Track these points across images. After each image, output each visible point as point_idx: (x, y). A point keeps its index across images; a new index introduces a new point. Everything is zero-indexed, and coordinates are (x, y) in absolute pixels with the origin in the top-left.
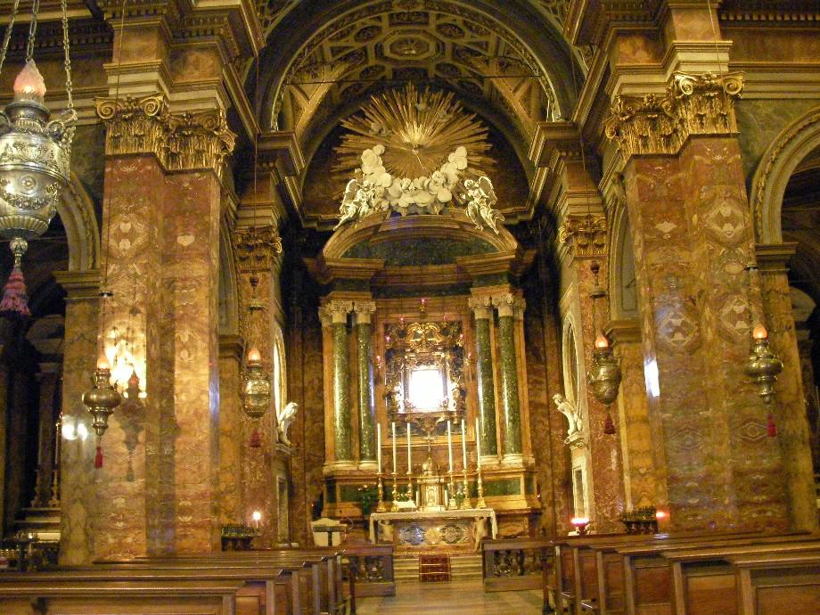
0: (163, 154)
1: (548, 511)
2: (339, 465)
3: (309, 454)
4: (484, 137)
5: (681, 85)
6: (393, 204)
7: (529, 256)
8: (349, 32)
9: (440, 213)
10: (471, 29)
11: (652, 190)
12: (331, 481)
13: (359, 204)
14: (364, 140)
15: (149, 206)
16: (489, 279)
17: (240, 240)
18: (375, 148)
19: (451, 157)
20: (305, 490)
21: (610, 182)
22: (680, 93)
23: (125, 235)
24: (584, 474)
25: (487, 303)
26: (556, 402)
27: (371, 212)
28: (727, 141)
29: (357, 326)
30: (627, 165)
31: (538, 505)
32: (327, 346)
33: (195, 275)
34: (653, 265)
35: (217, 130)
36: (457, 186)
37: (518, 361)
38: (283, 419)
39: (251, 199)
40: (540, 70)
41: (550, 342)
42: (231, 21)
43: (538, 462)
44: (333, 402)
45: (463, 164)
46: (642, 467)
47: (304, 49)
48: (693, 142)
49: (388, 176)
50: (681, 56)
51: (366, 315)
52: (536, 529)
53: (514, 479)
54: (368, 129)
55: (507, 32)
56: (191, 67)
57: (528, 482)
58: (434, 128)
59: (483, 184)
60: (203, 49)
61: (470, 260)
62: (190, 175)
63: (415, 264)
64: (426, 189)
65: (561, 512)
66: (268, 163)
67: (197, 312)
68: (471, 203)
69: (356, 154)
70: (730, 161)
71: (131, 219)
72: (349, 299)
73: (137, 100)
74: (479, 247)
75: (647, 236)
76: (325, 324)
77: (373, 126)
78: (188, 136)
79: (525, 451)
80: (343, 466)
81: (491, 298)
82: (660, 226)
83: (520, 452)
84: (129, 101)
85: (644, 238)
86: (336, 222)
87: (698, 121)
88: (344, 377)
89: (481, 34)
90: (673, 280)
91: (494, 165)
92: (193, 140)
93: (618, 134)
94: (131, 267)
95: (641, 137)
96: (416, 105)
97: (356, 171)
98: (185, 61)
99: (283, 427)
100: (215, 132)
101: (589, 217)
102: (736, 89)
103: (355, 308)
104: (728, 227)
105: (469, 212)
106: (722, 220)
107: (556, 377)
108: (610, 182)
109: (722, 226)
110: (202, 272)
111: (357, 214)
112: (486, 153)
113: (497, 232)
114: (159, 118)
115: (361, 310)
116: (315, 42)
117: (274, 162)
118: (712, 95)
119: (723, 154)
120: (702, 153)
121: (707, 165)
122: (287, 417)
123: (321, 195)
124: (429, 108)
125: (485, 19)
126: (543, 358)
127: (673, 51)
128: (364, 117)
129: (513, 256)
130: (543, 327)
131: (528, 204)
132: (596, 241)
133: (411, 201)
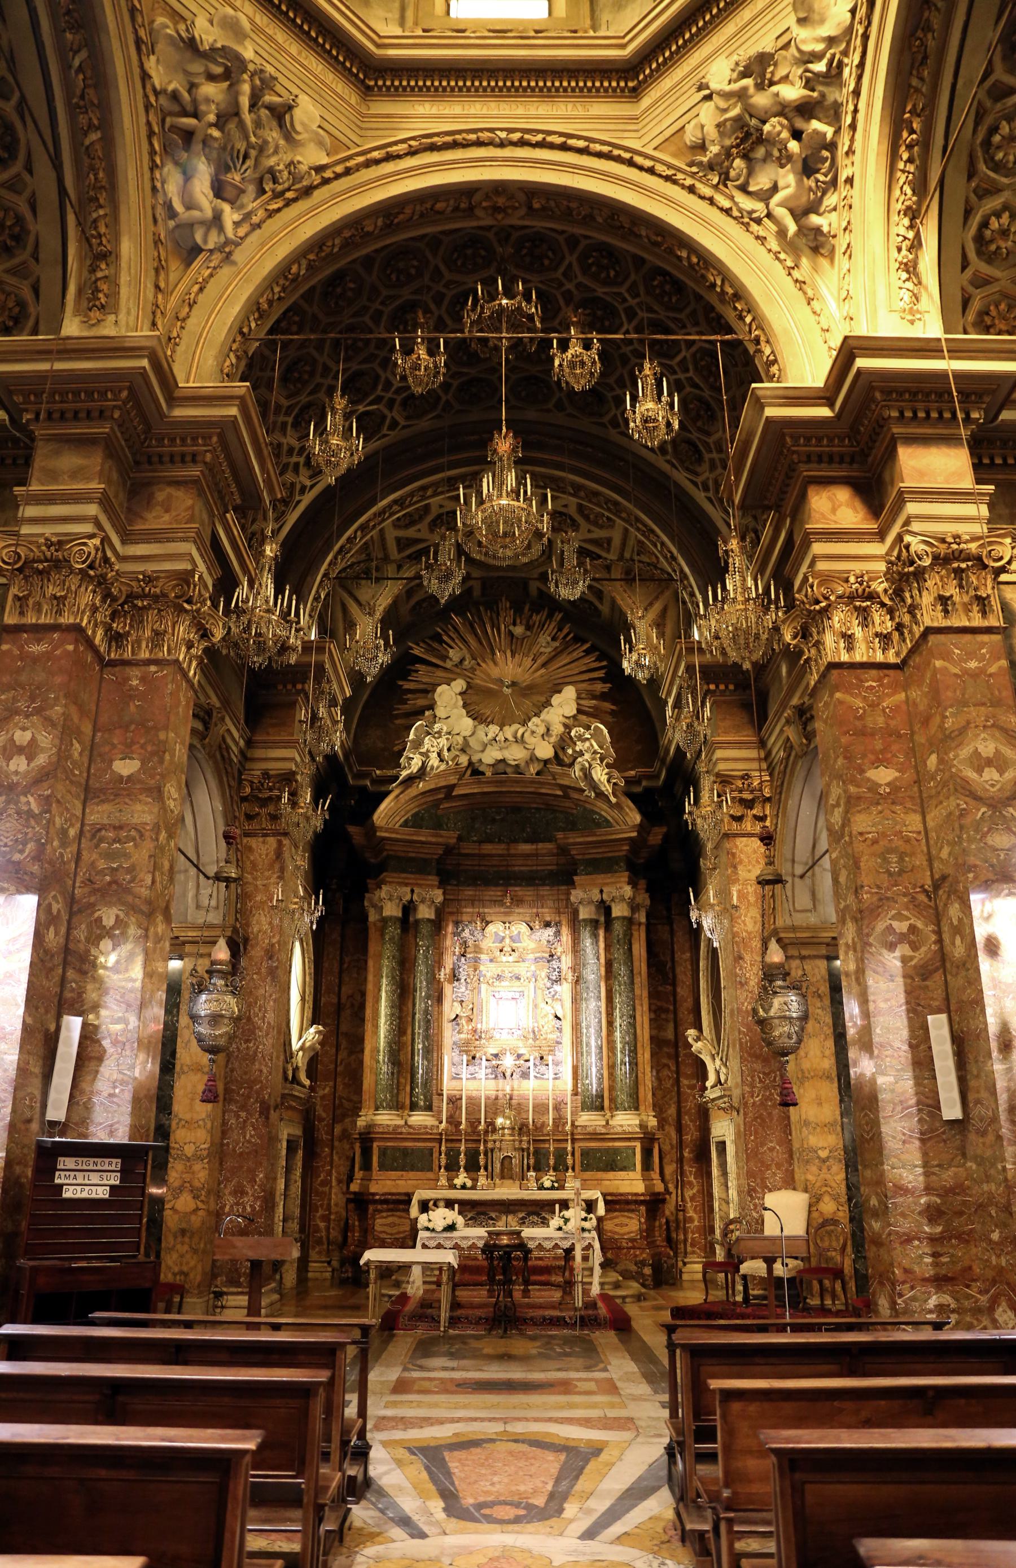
0: (100, 633)
1: (672, 1201)
2: (378, 1117)
3: (340, 1098)
4: (601, 674)
5: (912, 549)
6: (475, 759)
7: (657, 836)
8: (421, 518)
9: (538, 774)
10: (587, 518)
11: (861, 718)
12: (367, 1138)
13: (426, 755)
14: (440, 673)
15: (66, 706)
16: (600, 866)
17: (248, 790)
18: (453, 684)
19: (556, 699)
20: (332, 1148)
21: (783, 720)
22: (912, 563)
23: (20, 750)
24: (730, 1149)
25: (596, 896)
26: (690, 1040)
27: (443, 767)
28: (985, 638)
29: (417, 922)
30: (819, 682)
31: (659, 1187)
32: (373, 947)
33: (135, 821)
34: (861, 834)
35: (189, 602)
36: (562, 738)
37: (637, 980)
38: (302, 1048)
39: (268, 734)
40: (682, 571)
41: (683, 957)
42: (221, 436)
43: (662, 1122)
44: (376, 1026)
45: (571, 710)
46: (824, 1148)
47: (356, 532)
48: (932, 639)
49: (468, 723)
50: (912, 508)
51: (429, 907)
52: (657, 1223)
53: (628, 1147)
54: (445, 658)
55: (638, 520)
56: (158, 508)
57: (647, 1153)
58: (534, 660)
59: (597, 735)
60: (177, 483)
61: (575, 838)
62: (143, 668)
63: (500, 841)
64: (520, 741)
65: (692, 1199)
66: (294, 686)
67: (132, 880)
68: (580, 759)
69: (429, 691)
70: (993, 669)
71: (33, 725)
72: (406, 885)
73: (60, 543)
74: (590, 821)
75: (852, 789)
76: (373, 917)
77: (451, 653)
78: (144, 608)
79: (642, 1108)
80: (386, 1118)
81: (601, 891)
82: (872, 774)
83: (637, 1109)
84: (49, 544)
85: (845, 791)
86: (397, 778)
87: (939, 608)
88: (393, 992)
89: (601, 527)
90: (894, 858)
91: (612, 713)
92: (152, 615)
93: (804, 637)
94: (23, 799)
95: (844, 635)
96: (511, 628)
97: (427, 713)
98: (151, 497)
99: (301, 1060)
100: (186, 605)
101: (746, 777)
102: (1001, 558)
103: (415, 897)
104: (990, 774)
105: (577, 771)
106: (980, 763)
107: (689, 1003)
108: (783, 720)
109: (980, 771)
110: (148, 818)
111: (423, 767)
112: (603, 697)
113: (613, 800)
114: (92, 573)
115: (423, 901)
116: (372, 524)
117: (303, 683)
118: (963, 565)
119: (982, 659)
120: (946, 656)
121: (956, 675)
122: (308, 1044)
123: (380, 745)
124: (528, 633)
125: (608, 500)
126: (671, 975)
127: (901, 501)
128: (441, 641)
129: (635, 834)
130: (672, 932)
131: (657, 764)
132: (754, 812)
133: (499, 756)
